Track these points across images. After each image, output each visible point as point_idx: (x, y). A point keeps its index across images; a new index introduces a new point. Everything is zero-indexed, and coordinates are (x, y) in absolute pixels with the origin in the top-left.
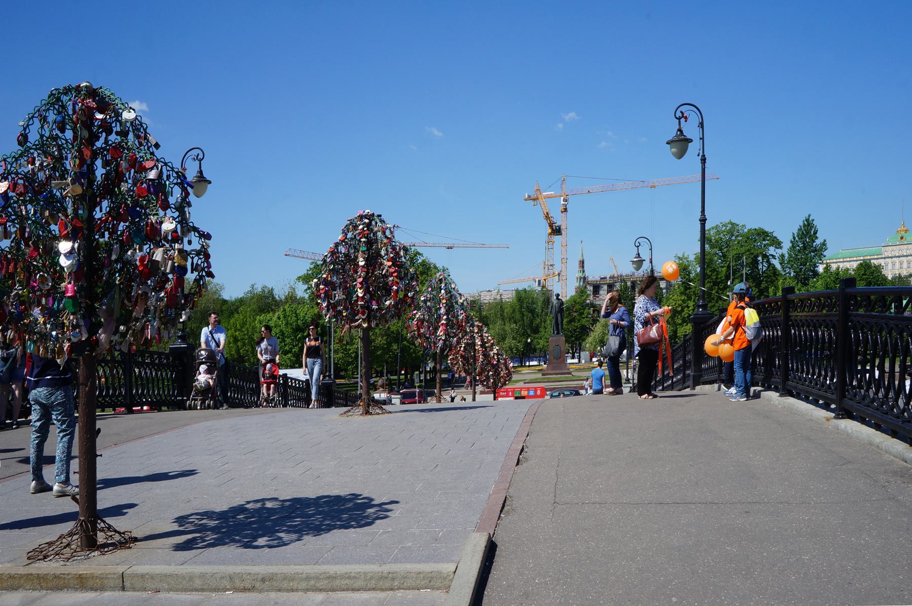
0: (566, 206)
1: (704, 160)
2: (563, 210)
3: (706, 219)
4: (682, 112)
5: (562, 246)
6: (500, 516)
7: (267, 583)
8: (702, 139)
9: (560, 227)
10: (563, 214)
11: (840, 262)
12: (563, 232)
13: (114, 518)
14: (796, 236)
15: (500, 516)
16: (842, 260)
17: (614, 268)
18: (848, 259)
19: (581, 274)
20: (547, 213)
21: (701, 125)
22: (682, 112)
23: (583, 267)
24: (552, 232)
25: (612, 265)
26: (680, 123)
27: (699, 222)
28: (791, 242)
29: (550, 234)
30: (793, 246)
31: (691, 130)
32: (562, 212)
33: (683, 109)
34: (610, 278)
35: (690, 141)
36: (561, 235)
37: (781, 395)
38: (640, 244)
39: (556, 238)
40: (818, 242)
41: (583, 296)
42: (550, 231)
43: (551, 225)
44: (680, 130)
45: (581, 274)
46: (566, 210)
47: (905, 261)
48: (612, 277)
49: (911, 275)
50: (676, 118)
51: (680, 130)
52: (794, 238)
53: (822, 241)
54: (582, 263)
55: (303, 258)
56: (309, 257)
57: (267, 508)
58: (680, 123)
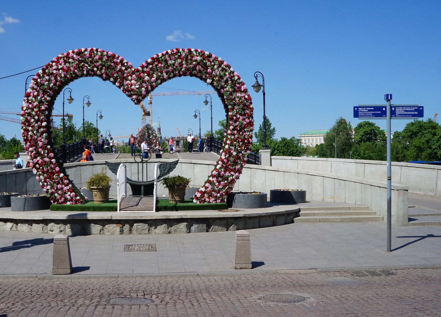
0: (151, 101)
1: (200, 119)
6: (108, 264)
9: (149, 113)
10: (150, 105)
11: (310, 136)
12: (151, 114)
14: (261, 125)
16: (311, 135)
17: (178, 133)
18: (315, 135)
20: (143, 105)
23: (160, 131)
24: (145, 114)
25: (178, 131)
28: (260, 128)
29: (144, 115)
30: (260, 129)
32: (149, 104)
34: (177, 138)
36: (150, 116)
39: (147, 117)
40: (272, 128)
41: (164, 145)
42: (144, 114)
43: (144, 111)
44: (196, 114)
46: (151, 103)
47: (307, 139)
48: (179, 138)
51: (196, 114)
53: (273, 128)
55: (7, 120)
56: (10, 120)
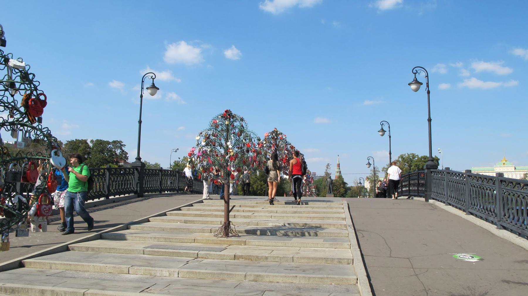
1: (390, 137)
3: (431, 120)
4: (416, 70)
7: (4, 273)
8: (389, 131)
13: (182, 196)
19: (338, 170)
22: (416, 70)
26: (382, 126)
27: (428, 121)
31: (386, 128)
33: (383, 122)
35: (421, 84)
37: (467, 214)
38: (417, 72)
45: (338, 170)
49: (525, 175)
50: (414, 73)
54: (339, 165)
57: (89, 215)
58: (382, 126)
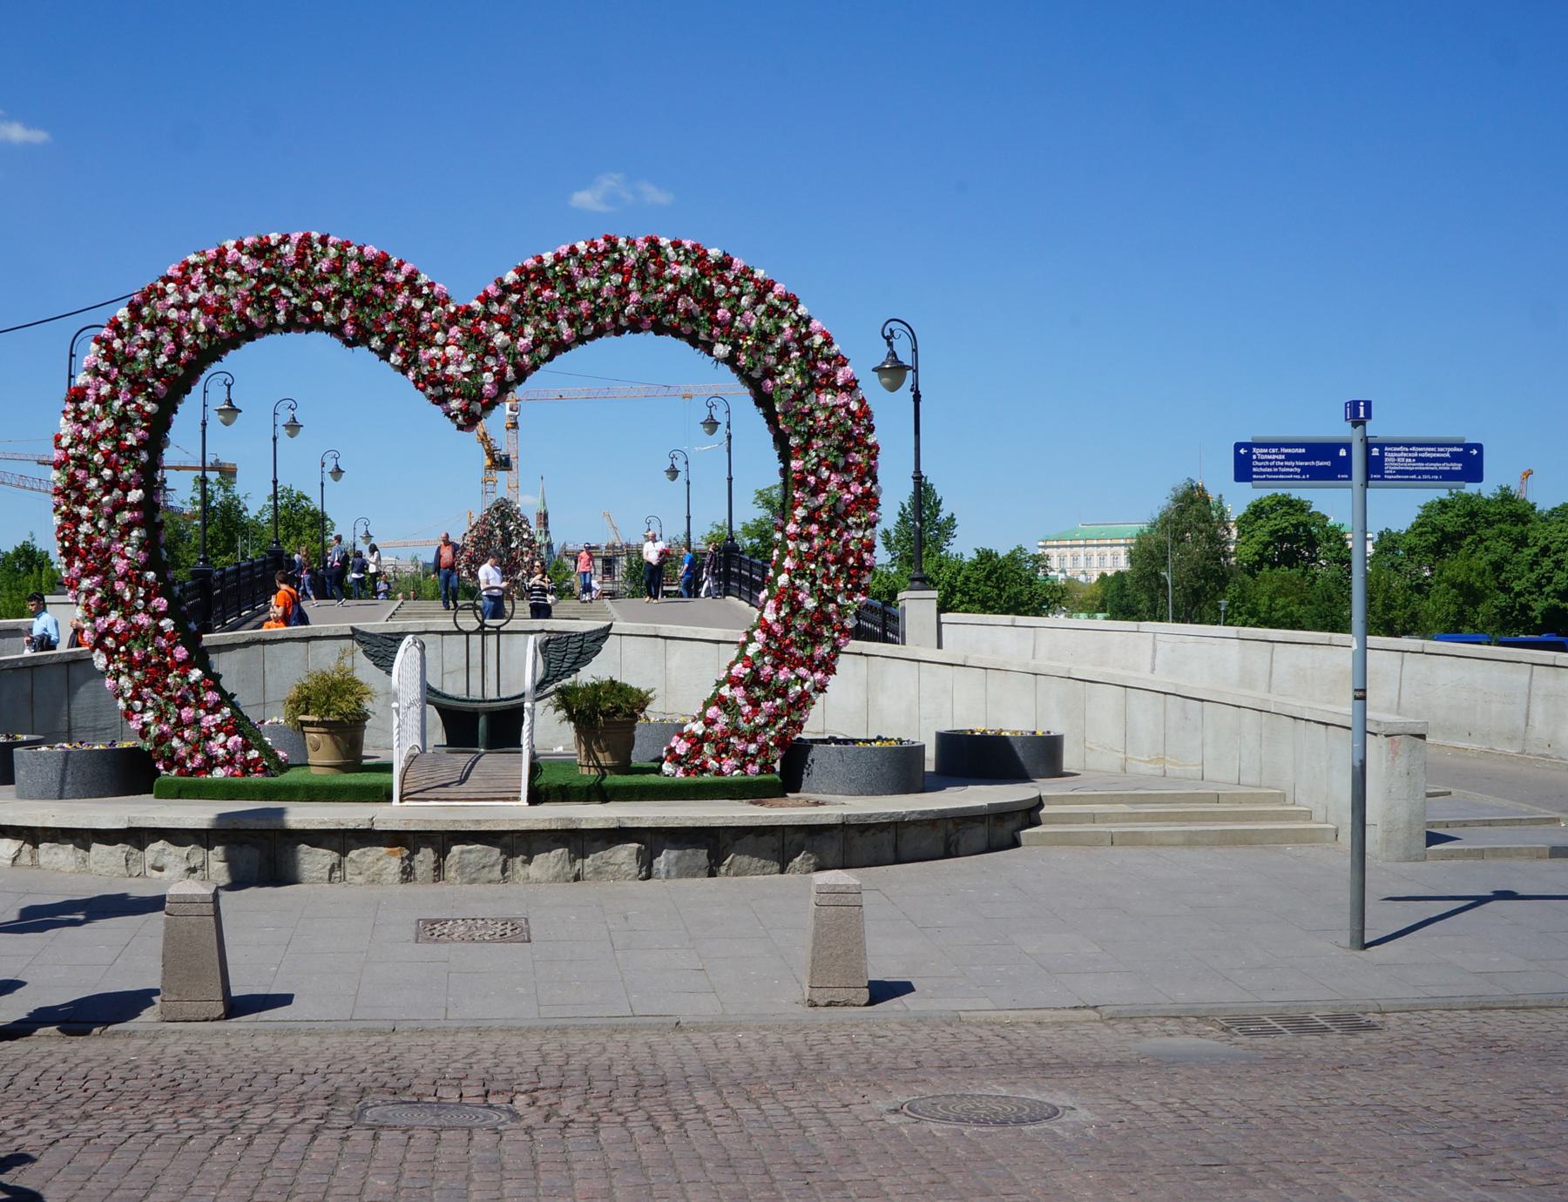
0: (516, 417)
1: (688, 483)
2: (509, 425)
5: (509, 487)
9: (508, 458)
11: (1080, 546)
12: (514, 466)
14: (906, 506)
15: (359, 985)
16: (1082, 542)
18: (1095, 542)
20: (485, 434)
21: (687, 463)
28: (900, 514)
29: (490, 467)
36: (511, 469)
39: (501, 475)
40: (943, 515)
41: (559, 574)
42: (488, 462)
43: (490, 454)
44: (673, 465)
46: (515, 425)
51: (673, 465)
52: (904, 509)
53: (949, 515)
